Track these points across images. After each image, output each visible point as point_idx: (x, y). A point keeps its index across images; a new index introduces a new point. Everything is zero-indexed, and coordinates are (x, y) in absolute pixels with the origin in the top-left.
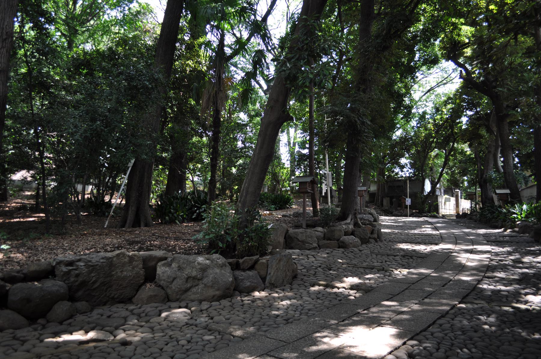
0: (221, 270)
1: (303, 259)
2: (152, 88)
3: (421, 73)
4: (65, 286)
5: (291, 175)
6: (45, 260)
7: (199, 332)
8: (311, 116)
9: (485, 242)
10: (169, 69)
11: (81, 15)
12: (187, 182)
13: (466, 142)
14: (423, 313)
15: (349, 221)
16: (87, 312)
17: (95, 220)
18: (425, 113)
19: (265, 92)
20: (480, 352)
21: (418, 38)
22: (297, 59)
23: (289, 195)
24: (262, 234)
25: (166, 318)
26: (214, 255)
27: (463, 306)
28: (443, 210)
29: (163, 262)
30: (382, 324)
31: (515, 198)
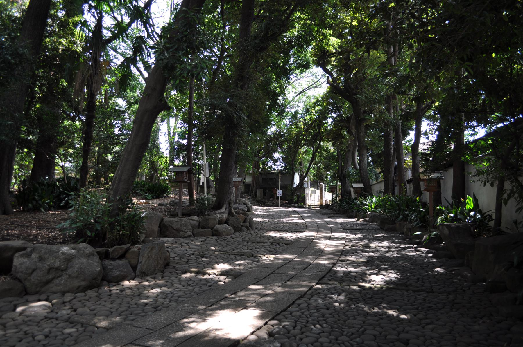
0: (88, 260)
1: (177, 247)
2: (16, 63)
3: (295, 75)
5: (170, 164)
7: (60, 325)
8: (190, 108)
9: (342, 230)
12: (56, 168)
13: (330, 141)
14: (284, 294)
15: (223, 210)
18: (297, 112)
19: (145, 79)
20: (330, 327)
22: (176, 50)
23: (167, 184)
24: (135, 221)
25: (21, 313)
26: (81, 244)
27: (319, 286)
28: (309, 202)
29: (21, 253)
30: (247, 306)
31: (367, 192)
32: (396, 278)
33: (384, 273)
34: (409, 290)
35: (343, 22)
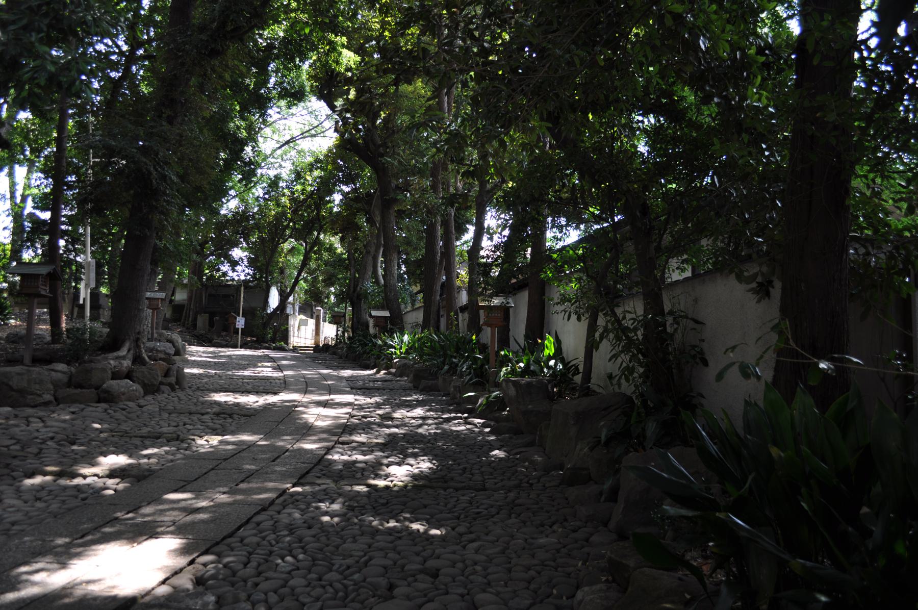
1: (16, 426)
3: (279, 110)
9: (348, 389)
13: (336, 234)
15: (123, 352)
18: (278, 178)
21: (276, 51)
22: (25, 28)
23: (5, 298)
27: (299, 489)
28: (296, 339)
30: (158, 533)
31: (394, 324)
32: (430, 469)
33: (411, 461)
34: (448, 488)
35: (365, 26)
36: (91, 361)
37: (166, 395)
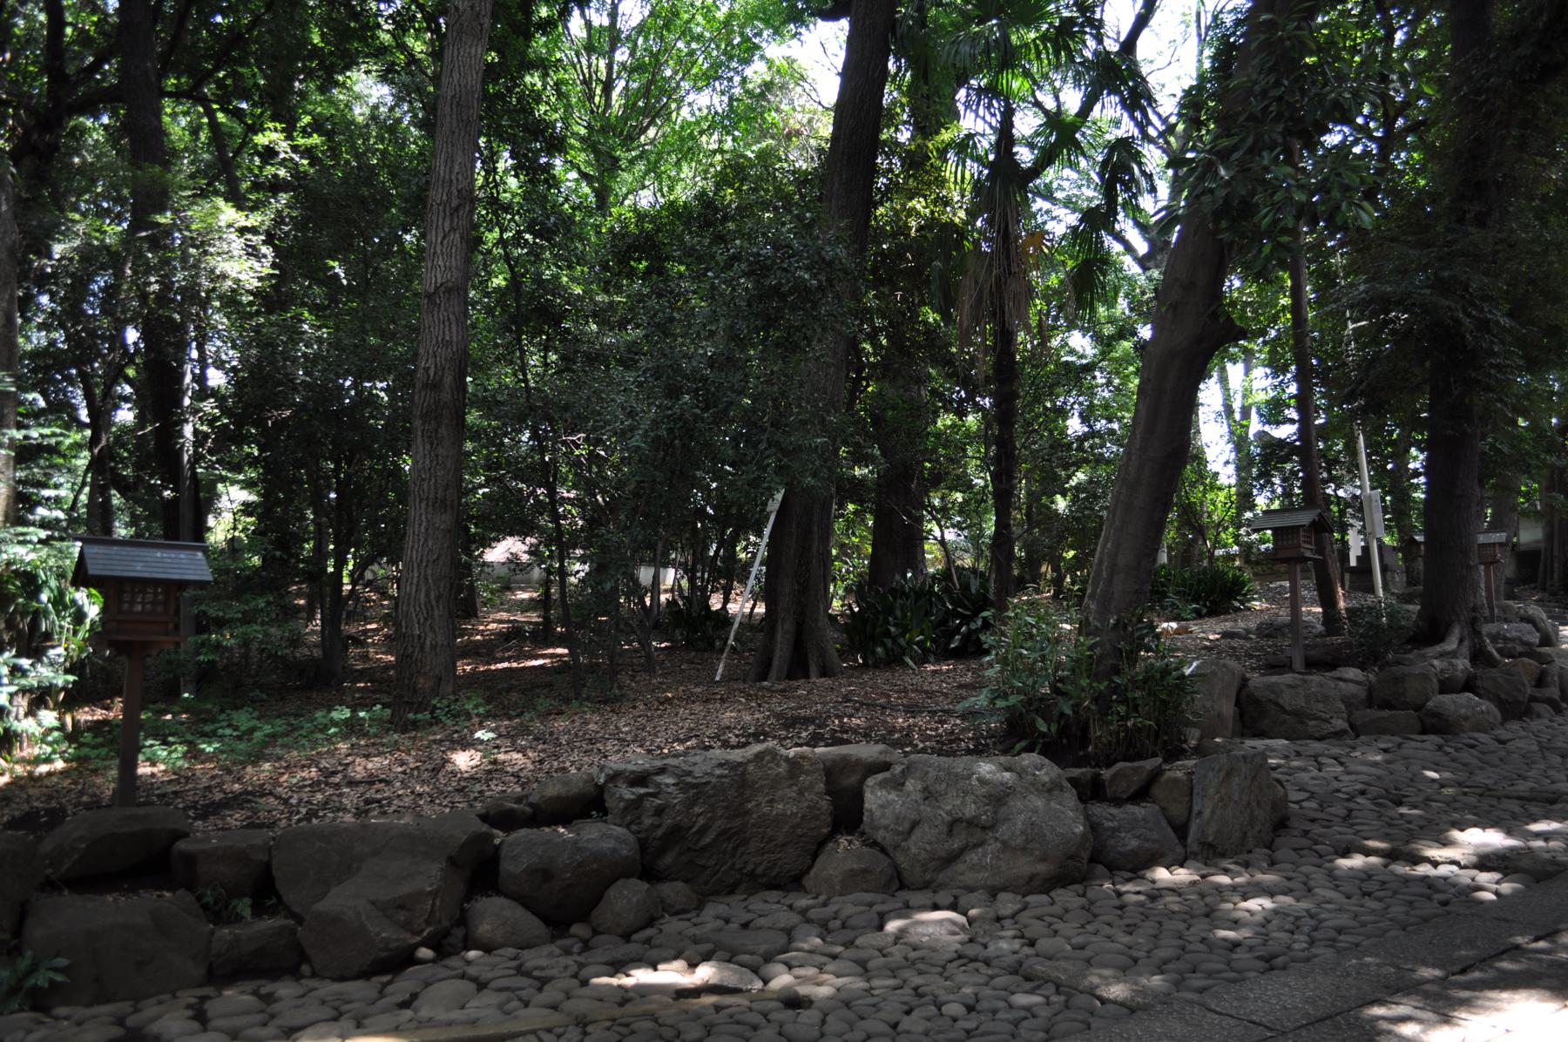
1: (1304, 770)
2: (820, 288)
4: (631, 838)
6: (579, 769)
10: (862, 232)
11: (624, 118)
15: (1451, 644)
16: (688, 912)
17: (690, 662)
19: (1143, 262)
22: (1250, 151)
23: (1239, 569)
24: (1168, 691)
25: (899, 936)
26: (1024, 755)
29: (880, 776)
36: (1399, 663)
37: (1546, 721)
